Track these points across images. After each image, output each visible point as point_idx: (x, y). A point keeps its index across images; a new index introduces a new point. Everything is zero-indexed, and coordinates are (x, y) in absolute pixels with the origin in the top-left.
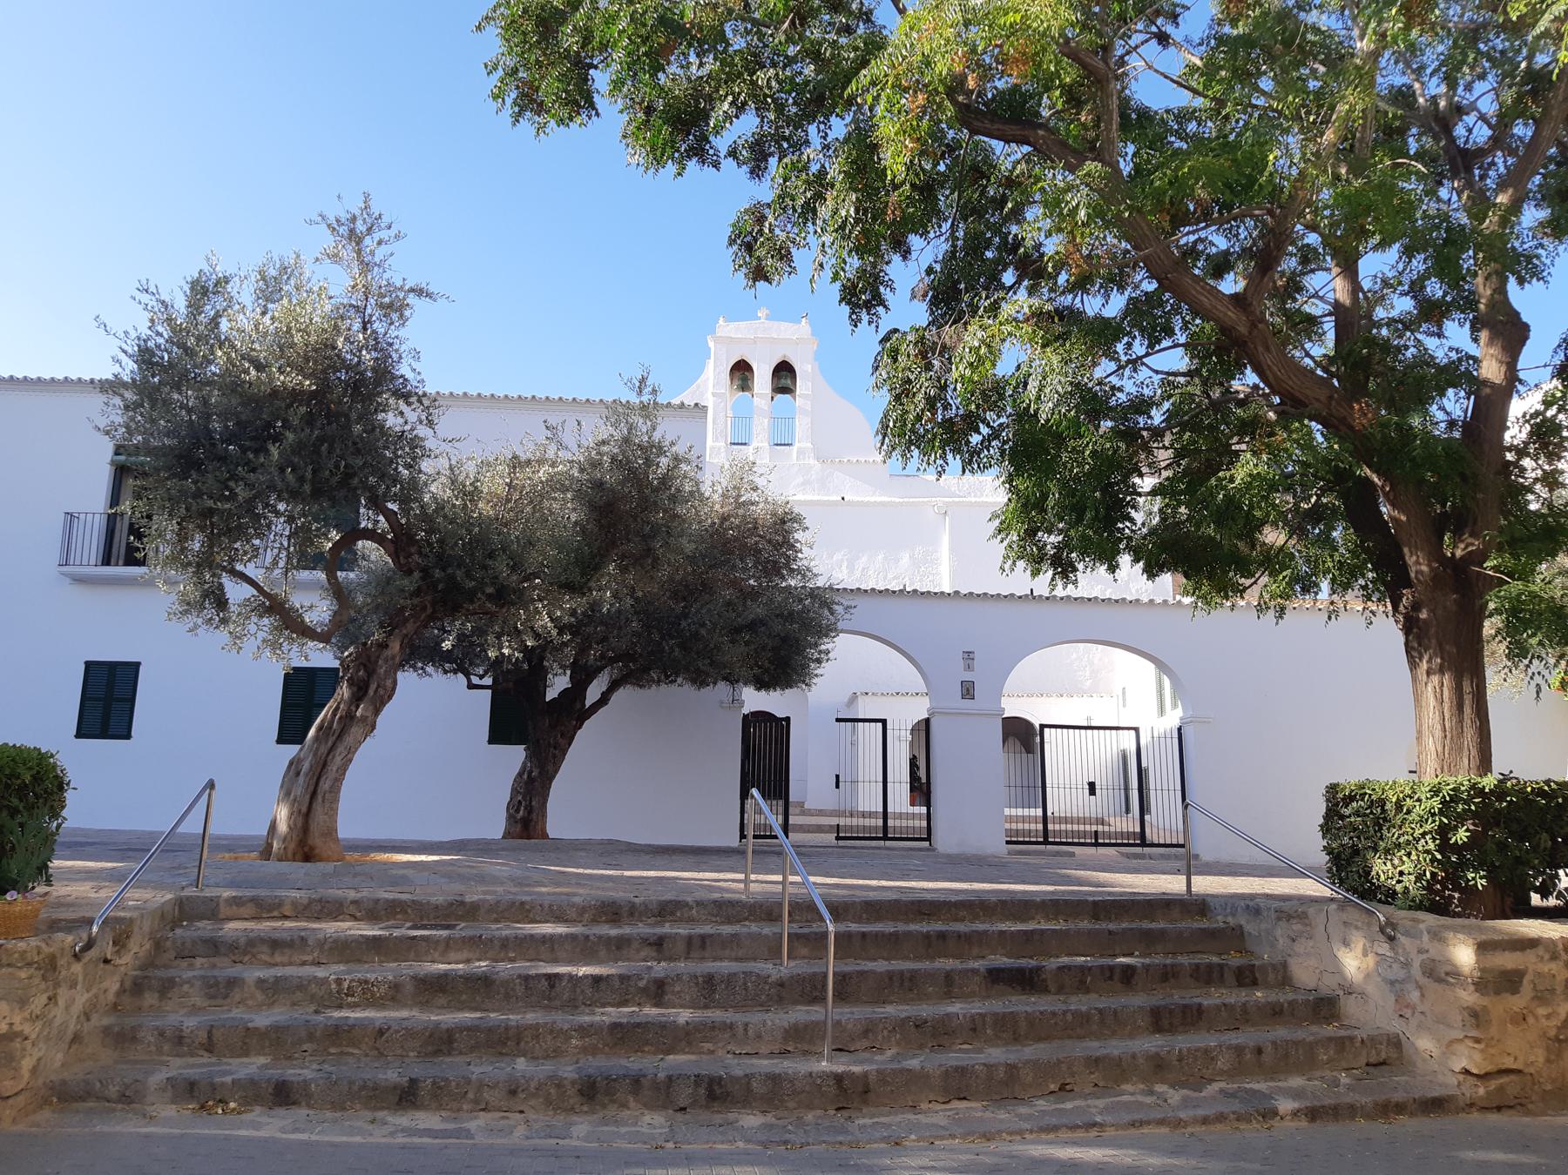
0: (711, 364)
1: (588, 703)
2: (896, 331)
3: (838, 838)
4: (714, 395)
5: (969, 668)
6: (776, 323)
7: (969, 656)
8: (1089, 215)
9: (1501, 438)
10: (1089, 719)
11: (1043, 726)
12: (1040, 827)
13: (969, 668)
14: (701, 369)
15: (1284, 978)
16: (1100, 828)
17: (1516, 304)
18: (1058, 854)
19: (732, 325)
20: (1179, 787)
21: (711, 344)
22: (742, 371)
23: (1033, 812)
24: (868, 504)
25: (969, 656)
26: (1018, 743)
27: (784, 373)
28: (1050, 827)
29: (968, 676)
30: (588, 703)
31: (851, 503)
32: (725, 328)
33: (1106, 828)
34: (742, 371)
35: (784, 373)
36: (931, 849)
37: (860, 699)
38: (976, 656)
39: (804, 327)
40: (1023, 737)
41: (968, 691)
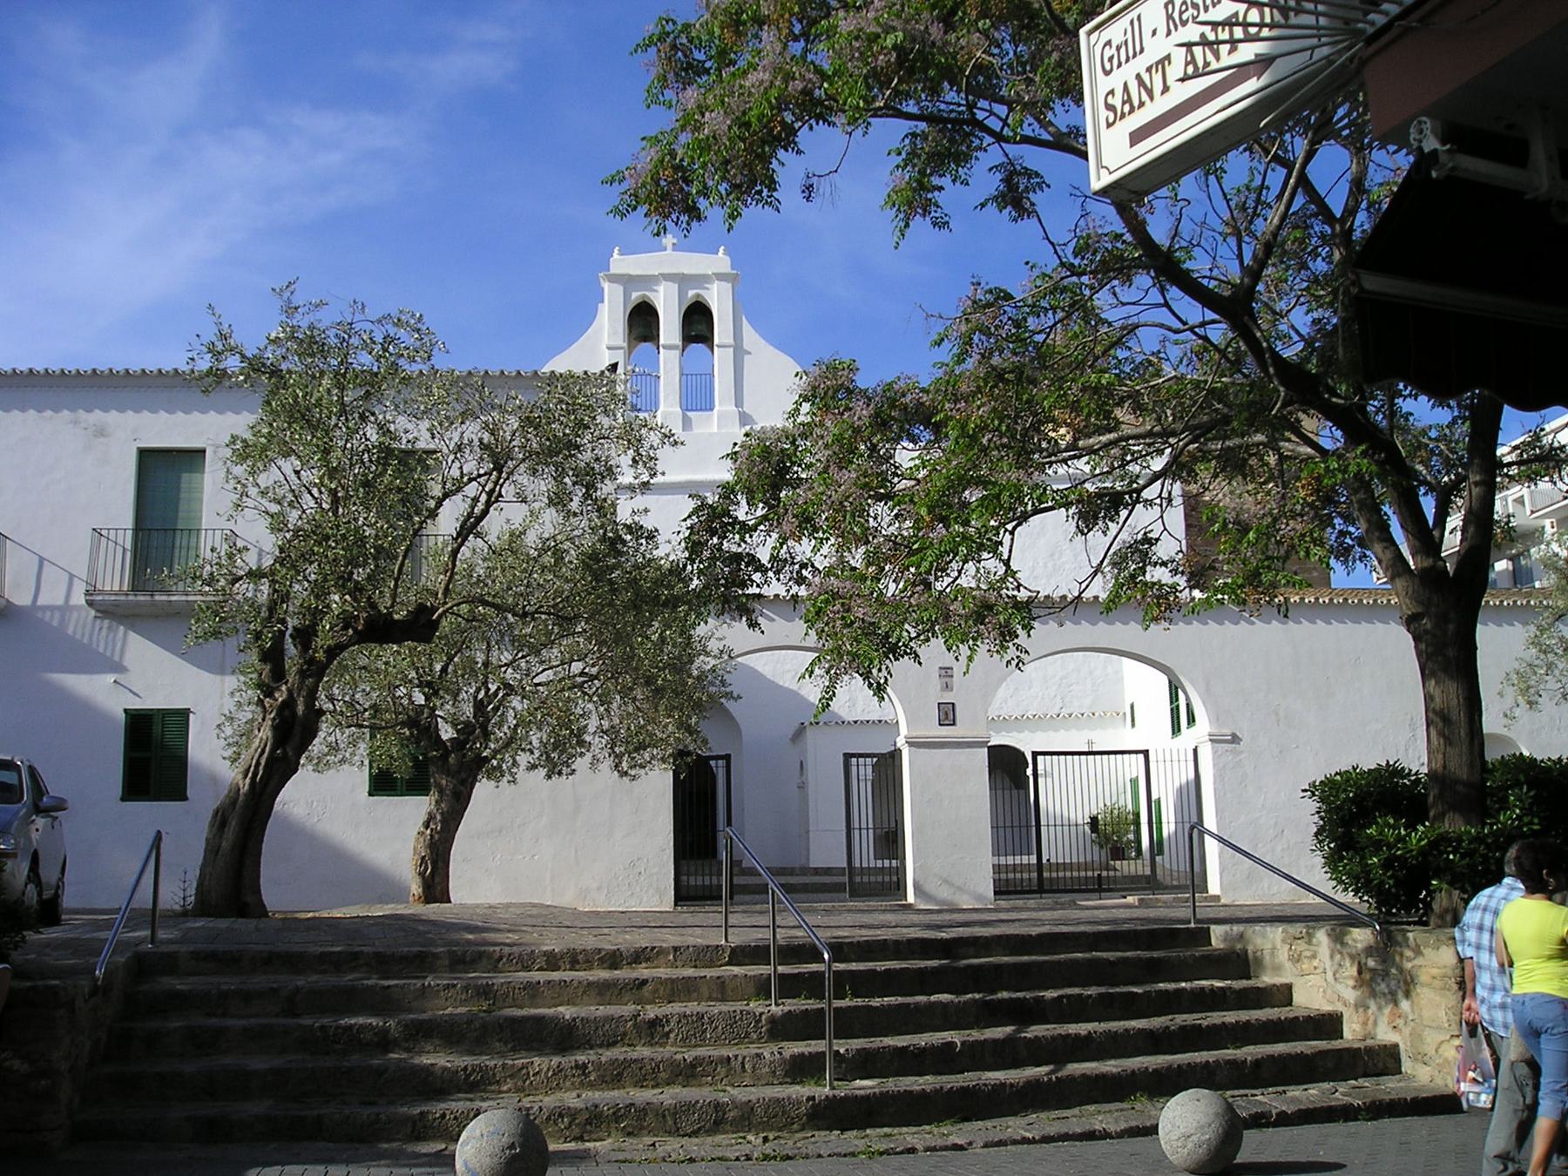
0: (604, 309)
1: (746, 327)
2: (1037, 175)
5: (947, 687)
9: (1473, 426)
11: (1035, 754)
12: (1035, 875)
14: (592, 315)
15: (1284, 995)
16: (1104, 874)
17: (461, 368)
23: (1025, 860)
26: (1007, 780)
27: (697, 321)
28: (1046, 874)
29: (948, 698)
30: (746, 327)
32: (621, 263)
33: (1112, 873)
34: (643, 320)
35: (697, 321)
37: (809, 733)
40: (1009, 768)
41: (947, 715)
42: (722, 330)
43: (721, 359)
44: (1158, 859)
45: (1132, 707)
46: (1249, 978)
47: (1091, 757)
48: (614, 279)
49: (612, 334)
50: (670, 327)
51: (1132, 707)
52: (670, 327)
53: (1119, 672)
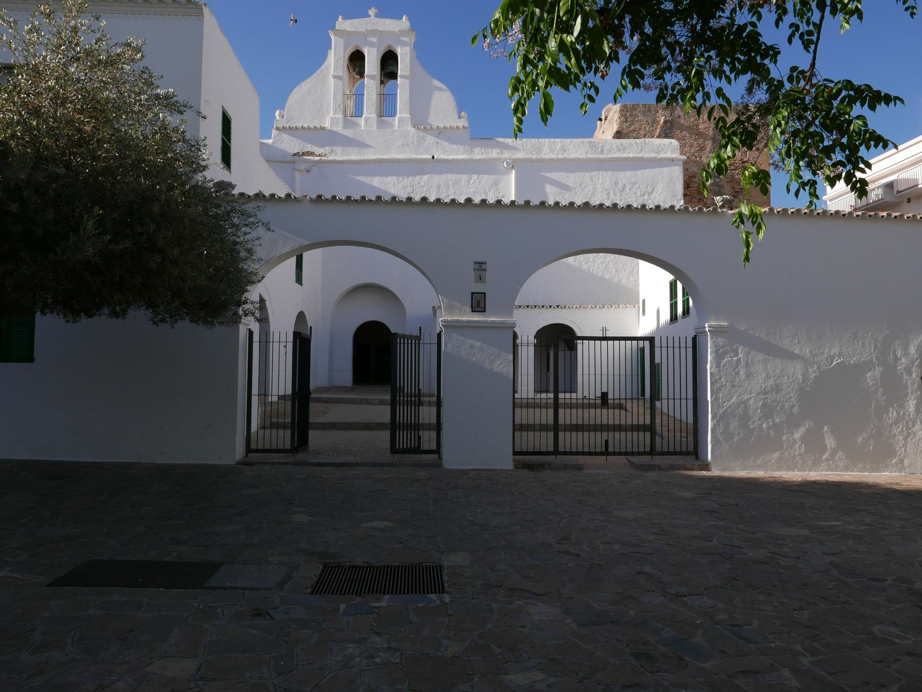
0: (332, 55)
3: (394, 450)
4: (334, 77)
5: (480, 279)
6: (383, 20)
7: (480, 267)
8: (887, 412)
10: (604, 330)
13: (480, 279)
14: (324, 57)
18: (565, 467)
19: (348, 22)
20: (690, 396)
21: (333, 37)
22: (356, 60)
24: (457, 161)
25: (480, 267)
27: (389, 60)
29: (479, 288)
31: (439, 161)
32: (342, 24)
34: (356, 60)
35: (389, 60)
36: (438, 465)
38: (488, 267)
39: (404, 23)
42: (403, 67)
43: (402, 84)
44: (658, 404)
45: (226, 123)
46: (709, 470)
47: (604, 343)
48: (340, 33)
49: (336, 68)
50: (372, 65)
51: (226, 123)
52: (372, 65)
53: (638, 264)
